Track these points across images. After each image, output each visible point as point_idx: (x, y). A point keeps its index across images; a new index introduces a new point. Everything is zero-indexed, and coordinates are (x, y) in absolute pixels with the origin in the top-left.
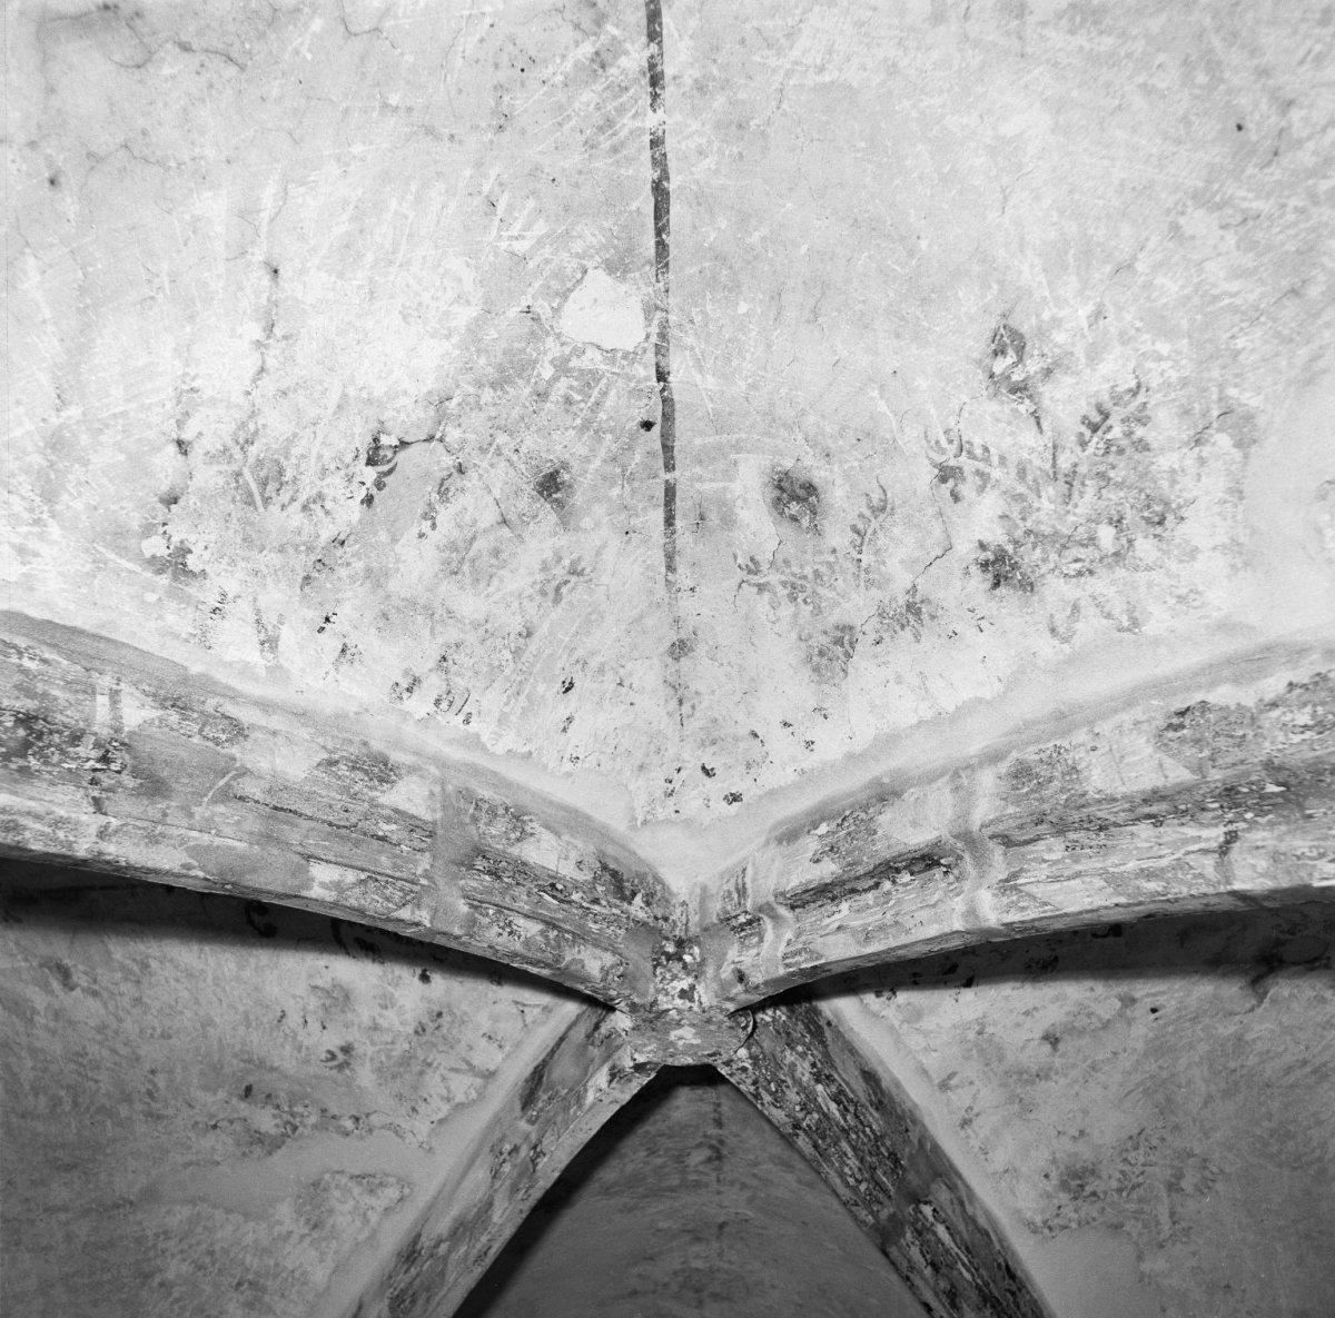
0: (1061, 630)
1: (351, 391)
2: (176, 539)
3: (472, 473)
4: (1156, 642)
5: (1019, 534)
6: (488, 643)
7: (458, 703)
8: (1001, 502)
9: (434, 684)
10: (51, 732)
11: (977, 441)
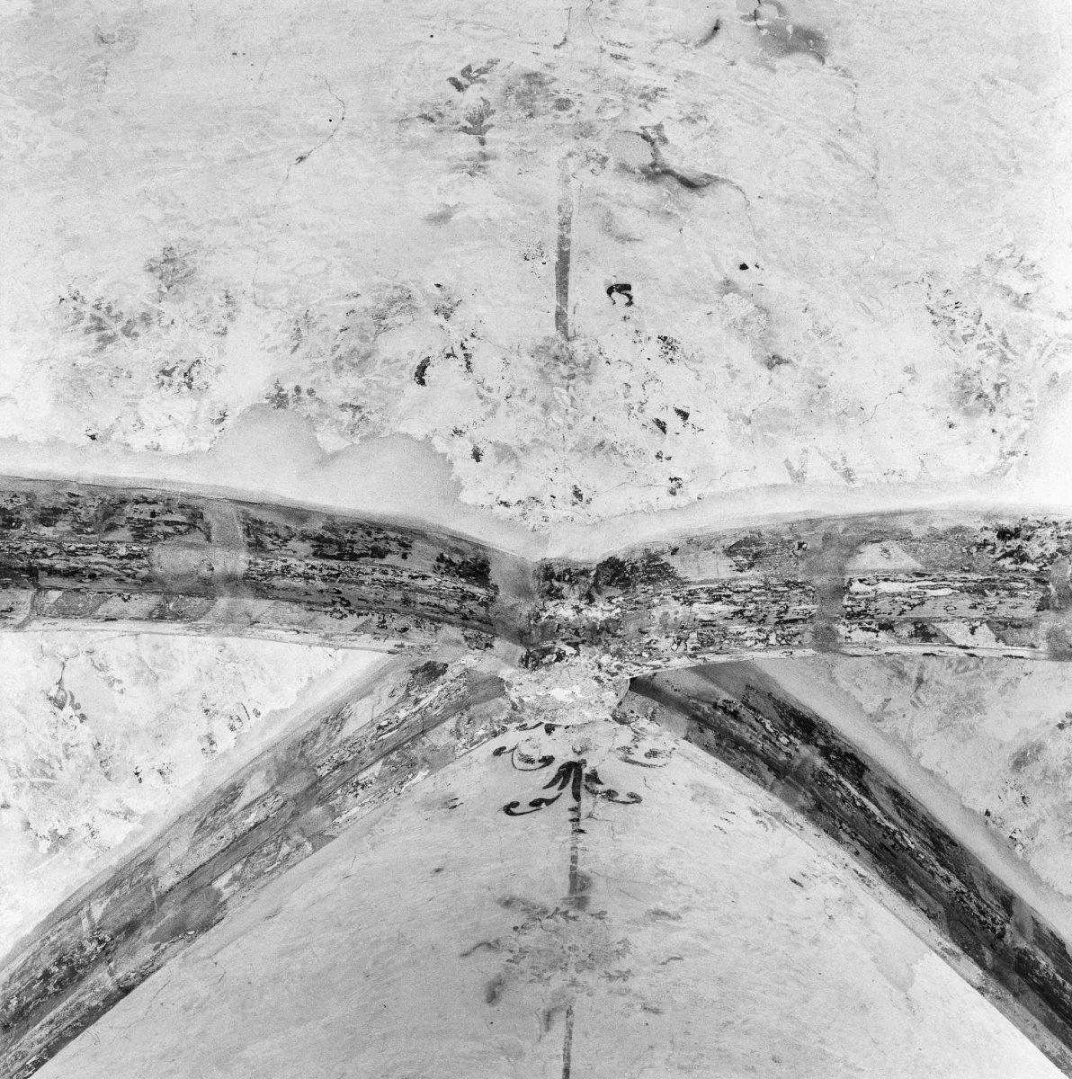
1: (17, 703)
2: (46, 834)
3: (96, 646)
6: (215, 675)
7: (242, 714)
9: (219, 726)
10: (72, 956)
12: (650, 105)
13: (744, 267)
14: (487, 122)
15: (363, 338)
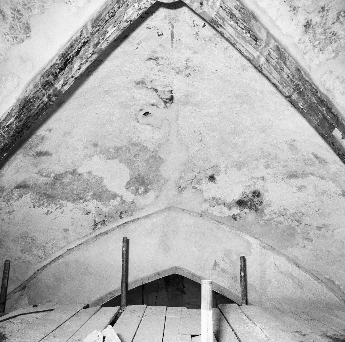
0: (300, 41)
4: (304, 58)
5: (314, 27)
8: (319, 22)
11: (329, 13)
12: (159, 69)
13: (137, 48)
14: (186, 67)
15: (215, 38)
